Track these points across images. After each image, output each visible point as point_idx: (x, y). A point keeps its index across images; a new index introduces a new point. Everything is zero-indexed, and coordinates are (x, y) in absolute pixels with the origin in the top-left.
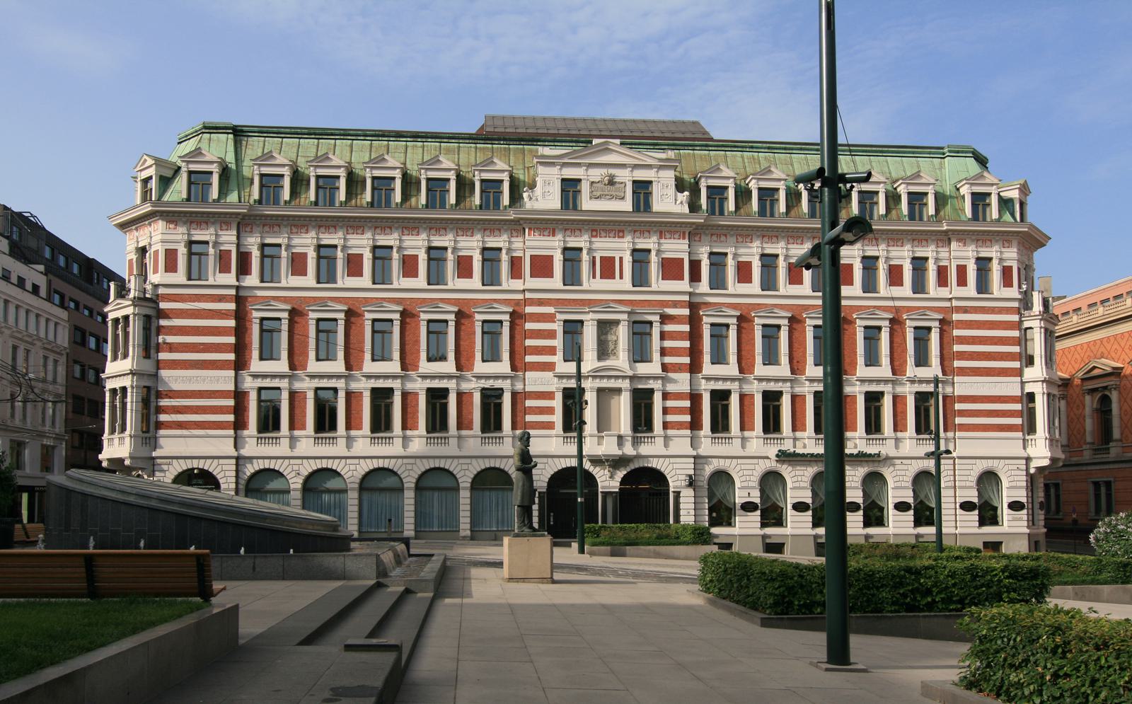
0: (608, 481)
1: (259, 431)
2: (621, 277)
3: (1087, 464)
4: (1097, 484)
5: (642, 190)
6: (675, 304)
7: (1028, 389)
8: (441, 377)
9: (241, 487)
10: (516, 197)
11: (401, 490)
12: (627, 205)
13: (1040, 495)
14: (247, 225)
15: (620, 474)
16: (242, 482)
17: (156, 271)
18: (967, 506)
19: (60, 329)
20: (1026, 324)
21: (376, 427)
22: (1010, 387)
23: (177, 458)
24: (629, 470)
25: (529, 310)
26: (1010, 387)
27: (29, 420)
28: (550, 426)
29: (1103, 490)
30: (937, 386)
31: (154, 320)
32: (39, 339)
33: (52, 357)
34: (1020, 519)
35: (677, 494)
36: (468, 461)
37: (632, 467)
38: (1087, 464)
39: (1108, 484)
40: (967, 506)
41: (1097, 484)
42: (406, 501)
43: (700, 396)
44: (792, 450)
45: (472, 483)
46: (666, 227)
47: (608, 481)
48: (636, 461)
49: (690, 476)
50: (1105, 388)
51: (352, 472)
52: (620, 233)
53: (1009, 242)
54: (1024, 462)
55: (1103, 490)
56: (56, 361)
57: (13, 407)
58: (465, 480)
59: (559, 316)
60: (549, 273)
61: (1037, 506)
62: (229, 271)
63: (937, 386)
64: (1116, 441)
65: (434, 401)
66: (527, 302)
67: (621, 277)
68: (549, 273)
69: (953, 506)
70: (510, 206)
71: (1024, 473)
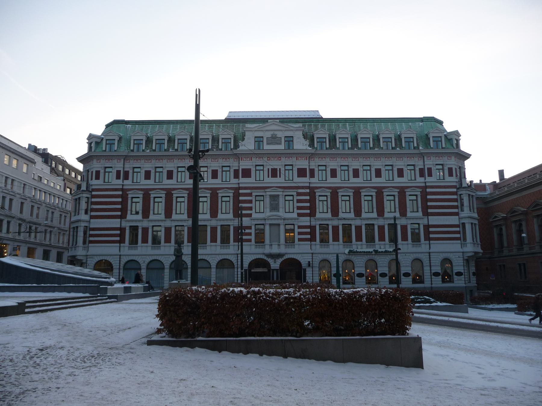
0: (275, 265)
1: (221, 243)
2: (280, 177)
3: (515, 255)
4: (520, 265)
5: (289, 140)
6: (303, 188)
7: (463, 221)
8: (326, 219)
9: (121, 267)
10: (236, 146)
11: (163, 269)
12: (282, 147)
13: (473, 269)
14: (127, 160)
15: (279, 261)
16: (122, 265)
17: (92, 179)
18: (436, 274)
19: (68, 203)
20: (459, 193)
21: (223, 242)
22: (454, 220)
23: (97, 255)
24: (283, 259)
25: (241, 191)
26: (454, 220)
27: (52, 241)
28: (250, 240)
29: (522, 267)
30: (395, 221)
31: (90, 199)
32: (58, 207)
33: (64, 215)
34: (461, 280)
35: (305, 270)
36: (168, 256)
37: (285, 258)
38: (515, 255)
39: (524, 264)
40: (436, 274)
41: (520, 265)
42: (165, 274)
43: (125, 229)
44: (355, 250)
45: (217, 266)
46: (300, 155)
47: (275, 265)
48: (286, 255)
49: (309, 262)
50: (520, 220)
51: (144, 262)
52: (279, 158)
53: (120, 160)
54: (462, 254)
55: (522, 267)
56: (65, 216)
57: (45, 234)
58: (214, 264)
59: (254, 194)
60: (249, 176)
61: (471, 274)
62: (120, 179)
63: (395, 221)
64: (527, 244)
65: (461, 226)
66: (240, 188)
67: (280, 177)
68: (249, 176)
69: (430, 274)
70: (233, 149)
71: (462, 259)
